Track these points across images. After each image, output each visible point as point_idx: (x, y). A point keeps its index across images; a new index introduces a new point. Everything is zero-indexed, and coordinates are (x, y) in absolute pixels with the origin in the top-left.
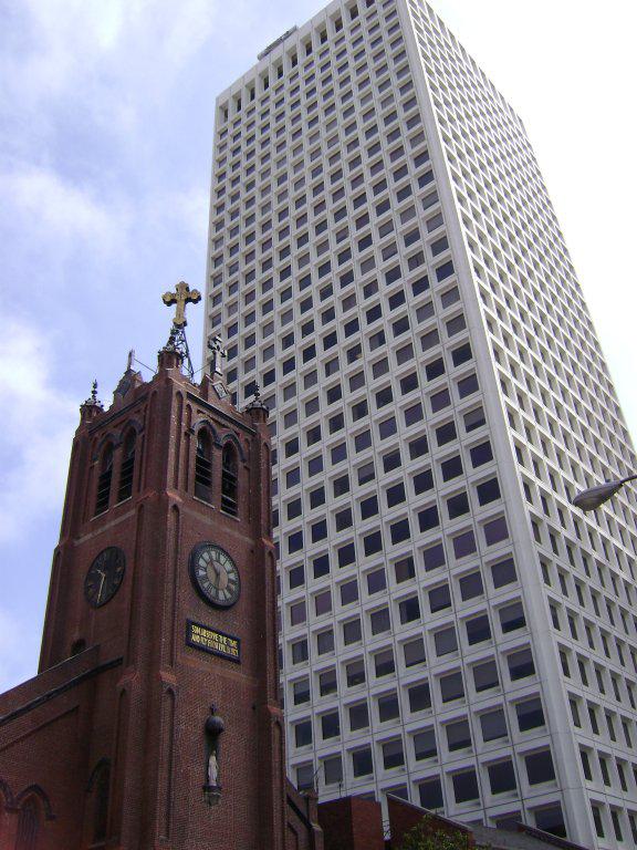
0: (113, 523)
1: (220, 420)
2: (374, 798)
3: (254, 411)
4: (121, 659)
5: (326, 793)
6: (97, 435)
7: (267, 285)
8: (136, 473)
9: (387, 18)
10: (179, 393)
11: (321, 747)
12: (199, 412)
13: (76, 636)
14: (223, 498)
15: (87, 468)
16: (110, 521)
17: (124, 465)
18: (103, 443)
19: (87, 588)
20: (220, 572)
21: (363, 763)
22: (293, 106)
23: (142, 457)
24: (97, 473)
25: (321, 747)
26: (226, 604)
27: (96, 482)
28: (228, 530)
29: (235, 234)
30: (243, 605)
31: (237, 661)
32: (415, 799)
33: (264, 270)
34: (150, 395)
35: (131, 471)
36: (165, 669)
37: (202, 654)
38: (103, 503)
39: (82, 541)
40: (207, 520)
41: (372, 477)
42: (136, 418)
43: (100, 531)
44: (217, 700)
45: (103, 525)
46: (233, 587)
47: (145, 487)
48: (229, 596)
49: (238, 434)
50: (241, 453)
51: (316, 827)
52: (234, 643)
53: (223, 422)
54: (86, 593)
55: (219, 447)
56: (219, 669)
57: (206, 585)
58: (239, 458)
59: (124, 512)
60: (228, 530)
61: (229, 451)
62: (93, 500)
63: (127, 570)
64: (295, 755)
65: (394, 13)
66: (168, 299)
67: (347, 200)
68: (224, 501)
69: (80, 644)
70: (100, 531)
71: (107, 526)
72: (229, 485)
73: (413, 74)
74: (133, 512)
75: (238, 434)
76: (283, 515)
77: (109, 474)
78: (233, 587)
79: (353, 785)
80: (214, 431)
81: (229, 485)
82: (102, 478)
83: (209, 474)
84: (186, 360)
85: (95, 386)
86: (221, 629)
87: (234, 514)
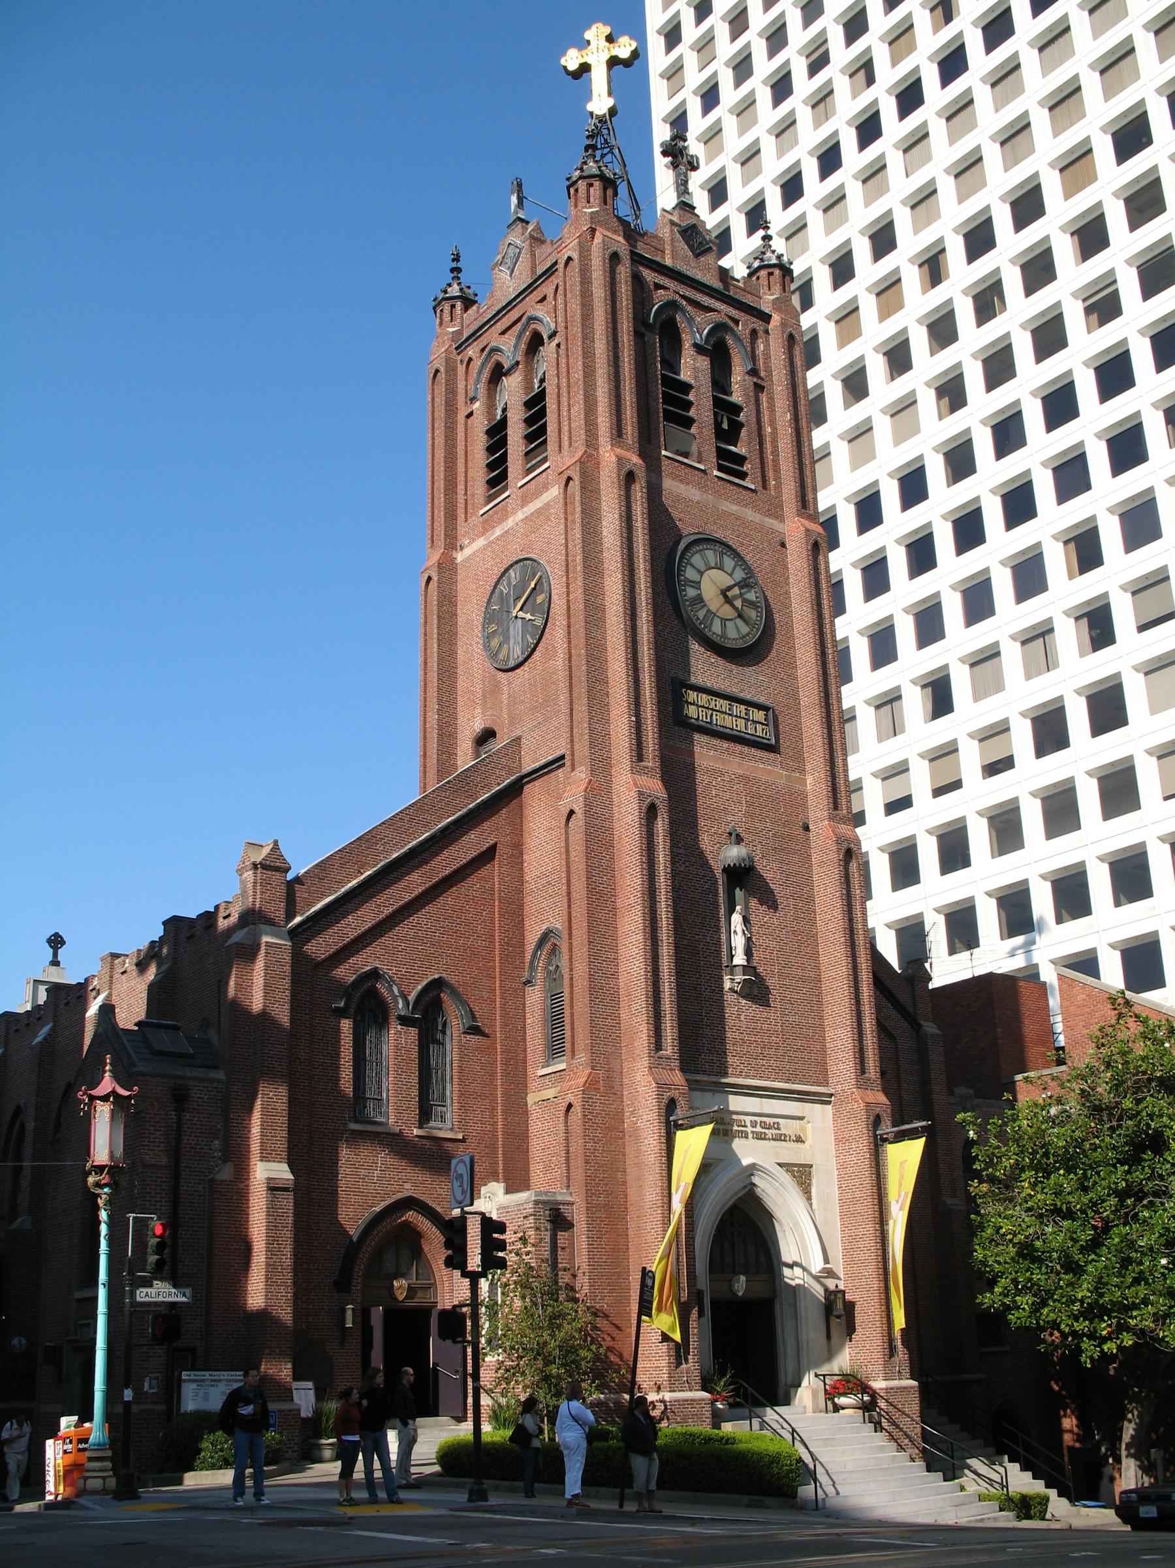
0: (520, 516)
2: (1037, 975)
4: (562, 757)
5: (947, 969)
6: (470, 352)
8: (551, 419)
11: (934, 893)
13: (478, 726)
14: (718, 448)
15: (461, 416)
16: (514, 512)
17: (528, 405)
18: (483, 365)
19: (488, 638)
21: (1016, 912)
23: (558, 387)
24: (480, 424)
25: (934, 893)
26: (740, 645)
27: (480, 441)
28: (734, 508)
32: (1112, 974)
34: (561, 266)
35: (542, 413)
37: (665, 1173)
38: (498, 477)
39: (467, 552)
41: (1007, 763)
42: (540, 312)
43: (498, 532)
45: (504, 518)
47: (570, 445)
48: (745, 629)
51: (930, 1028)
52: (759, 715)
54: (487, 647)
59: (538, 494)
60: (734, 508)
62: (479, 474)
63: (554, 597)
64: (885, 909)
68: (722, 454)
69: (486, 736)
70: (498, 532)
71: (510, 523)
74: (555, 491)
75: (736, 322)
76: (834, 394)
77: (502, 424)
79: (995, 954)
82: (490, 432)
83: (688, 405)
84: (623, 189)
85: (457, 259)
86: (734, 691)
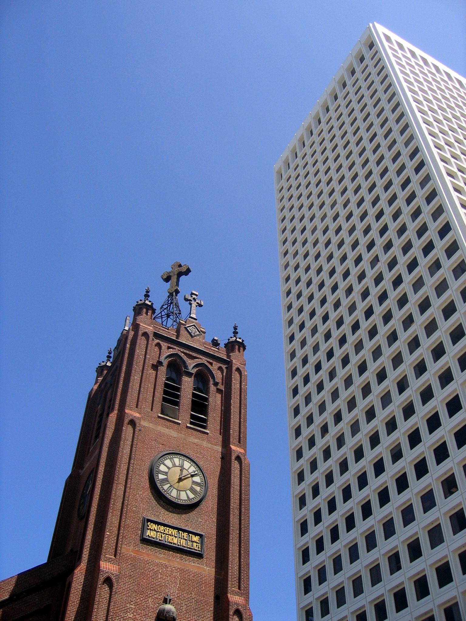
1: (191, 353)
3: (230, 345)
7: (387, 317)
9: (393, 111)
10: (145, 334)
12: (169, 348)
14: (192, 415)
20: (183, 478)
22: (345, 206)
28: (196, 441)
29: (350, 293)
30: (211, 503)
31: (199, 556)
33: (429, 335)
36: (109, 560)
40: (173, 433)
44: (172, 591)
46: (198, 489)
49: (211, 364)
50: (213, 377)
52: (196, 539)
53: (194, 354)
55: (189, 374)
56: (177, 562)
57: (166, 487)
58: (211, 382)
61: (202, 377)
65: (398, 105)
66: (165, 277)
67: (396, 250)
72: (200, 405)
73: (450, 214)
78: (198, 489)
80: (184, 362)
81: (200, 405)
87: (205, 427)
